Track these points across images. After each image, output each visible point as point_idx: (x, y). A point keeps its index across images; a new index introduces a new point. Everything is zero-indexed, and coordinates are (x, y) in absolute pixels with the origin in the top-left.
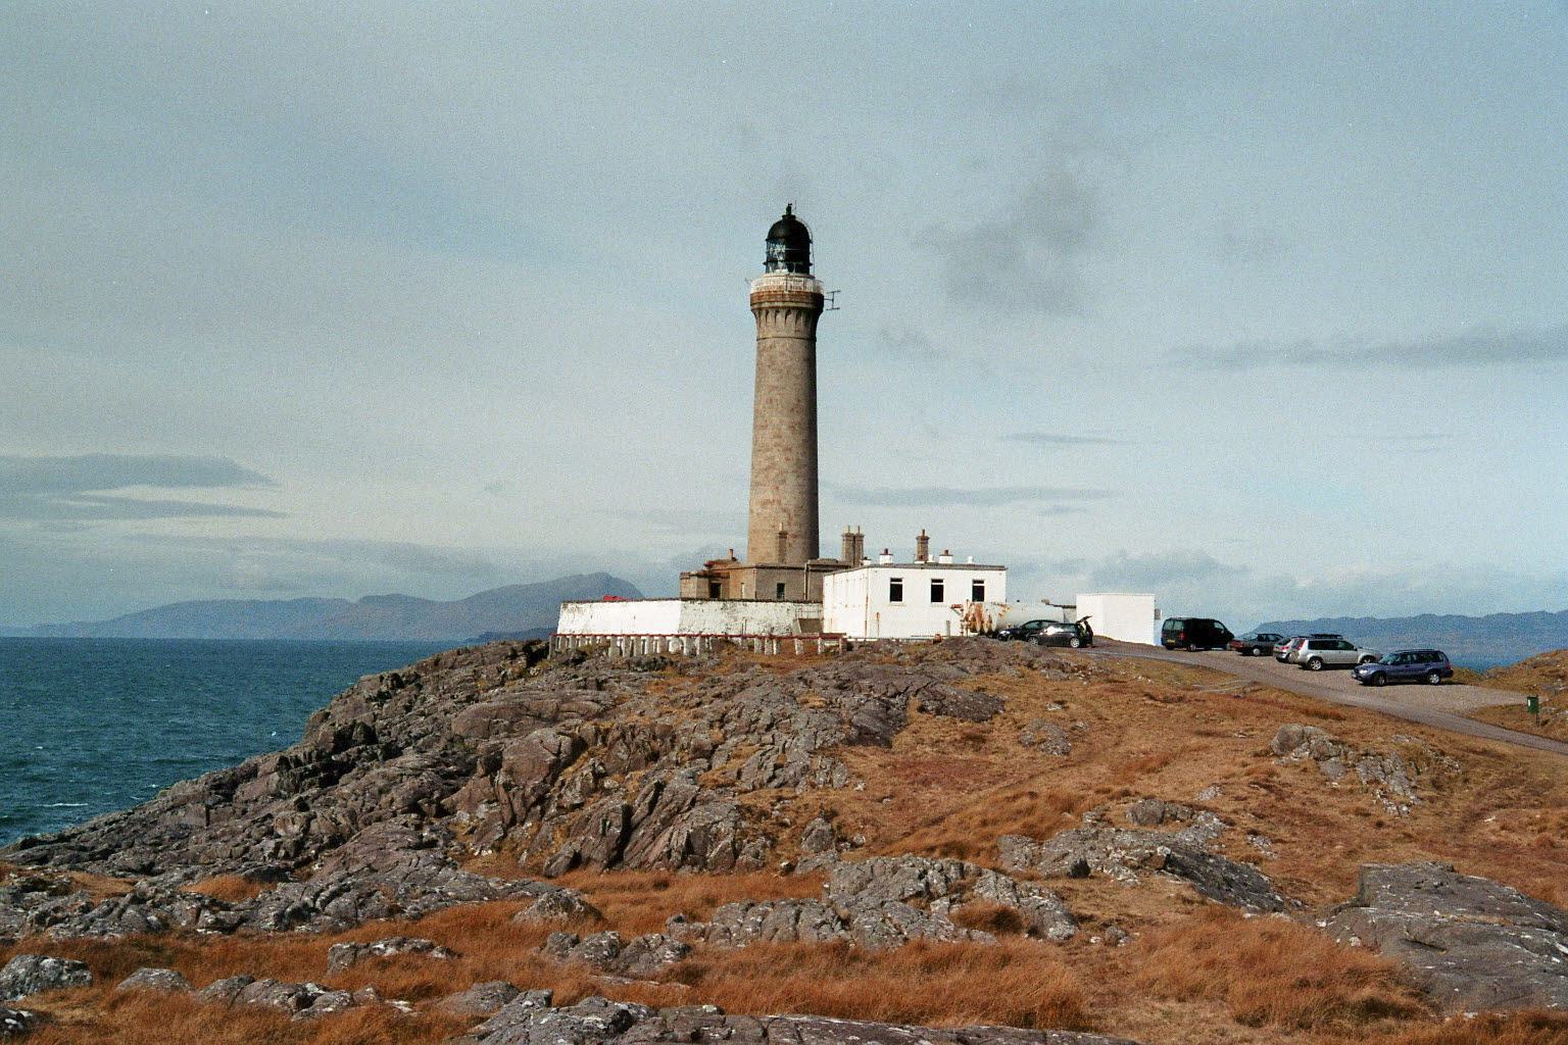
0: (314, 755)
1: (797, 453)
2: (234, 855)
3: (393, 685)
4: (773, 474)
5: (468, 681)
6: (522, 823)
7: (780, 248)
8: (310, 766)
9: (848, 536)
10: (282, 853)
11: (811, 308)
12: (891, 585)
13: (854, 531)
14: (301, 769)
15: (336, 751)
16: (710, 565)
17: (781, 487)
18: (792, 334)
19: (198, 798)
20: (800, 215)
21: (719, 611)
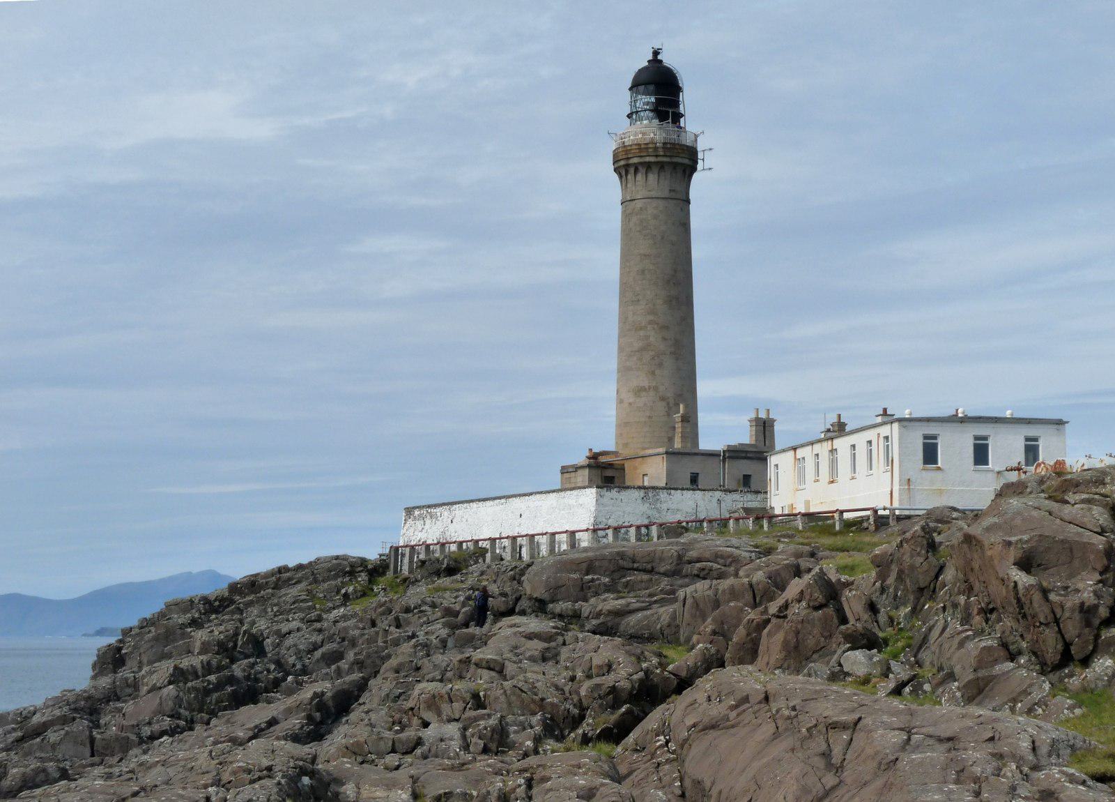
2: (399, 746)
3: (205, 609)
4: (647, 356)
5: (302, 601)
6: (1086, 662)
9: (757, 420)
11: (678, 162)
12: (924, 444)
13: (763, 415)
17: (657, 372)
18: (666, 194)
20: (667, 59)
21: (639, 501)
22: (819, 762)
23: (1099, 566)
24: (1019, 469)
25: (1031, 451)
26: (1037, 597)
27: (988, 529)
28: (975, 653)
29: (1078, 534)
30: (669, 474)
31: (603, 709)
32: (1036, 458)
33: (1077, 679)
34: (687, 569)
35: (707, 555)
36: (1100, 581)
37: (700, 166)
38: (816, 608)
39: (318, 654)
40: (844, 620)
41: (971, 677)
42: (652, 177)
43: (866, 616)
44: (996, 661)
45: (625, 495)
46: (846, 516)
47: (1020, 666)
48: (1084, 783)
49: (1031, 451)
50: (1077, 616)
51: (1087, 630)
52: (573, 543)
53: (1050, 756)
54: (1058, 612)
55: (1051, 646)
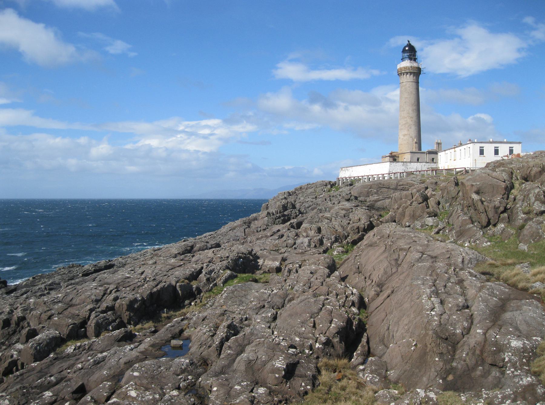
0: (279, 211)
1: (415, 119)
4: (407, 126)
6: (495, 225)
7: (406, 55)
8: (278, 215)
10: (313, 245)
14: (274, 217)
15: (284, 211)
16: (391, 154)
19: (241, 226)
22: (393, 263)
23: (502, 193)
24: (507, 156)
25: (511, 151)
26: (480, 203)
27: (468, 180)
28: (461, 221)
29: (497, 182)
30: (411, 158)
31: (354, 233)
32: (513, 153)
33: (491, 230)
34: (399, 187)
35: (405, 183)
36: (503, 198)
37: (422, 72)
38: (420, 204)
39: (310, 208)
40: (428, 207)
41: (458, 229)
42: (412, 76)
43: (435, 206)
44: (467, 224)
45: (398, 164)
46: (457, 170)
47: (475, 226)
48: (475, 276)
49: (511, 151)
50: (493, 210)
51: (496, 215)
52: (384, 178)
53: (468, 264)
54: (487, 208)
55: (484, 221)
